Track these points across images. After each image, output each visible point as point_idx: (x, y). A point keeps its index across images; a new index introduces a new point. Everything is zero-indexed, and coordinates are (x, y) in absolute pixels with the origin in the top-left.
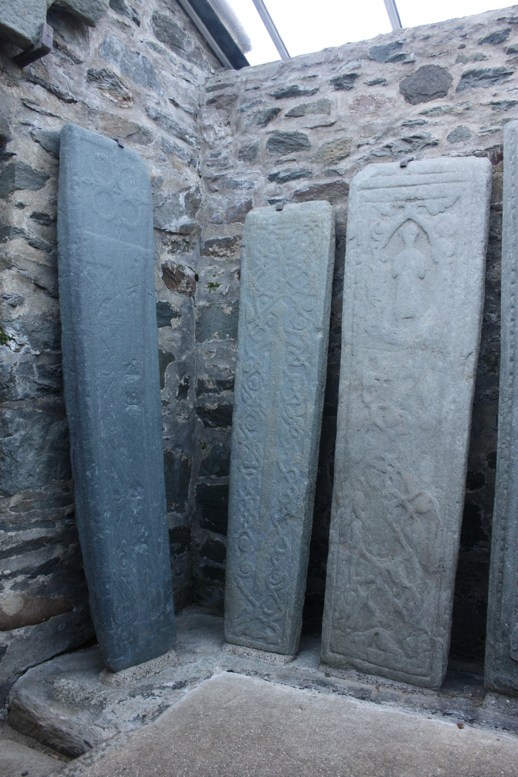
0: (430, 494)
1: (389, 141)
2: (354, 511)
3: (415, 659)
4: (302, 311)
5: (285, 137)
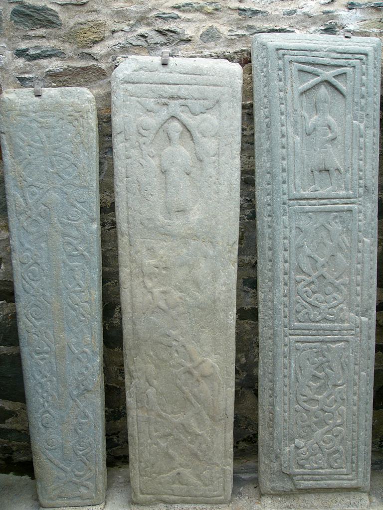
0: (211, 360)
1: (143, 30)
2: (147, 381)
3: (211, 486)
4: (75, 202)
5: (32, 10)
